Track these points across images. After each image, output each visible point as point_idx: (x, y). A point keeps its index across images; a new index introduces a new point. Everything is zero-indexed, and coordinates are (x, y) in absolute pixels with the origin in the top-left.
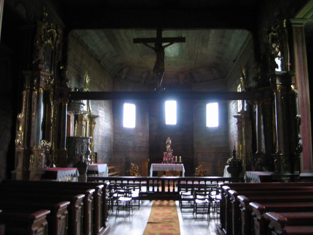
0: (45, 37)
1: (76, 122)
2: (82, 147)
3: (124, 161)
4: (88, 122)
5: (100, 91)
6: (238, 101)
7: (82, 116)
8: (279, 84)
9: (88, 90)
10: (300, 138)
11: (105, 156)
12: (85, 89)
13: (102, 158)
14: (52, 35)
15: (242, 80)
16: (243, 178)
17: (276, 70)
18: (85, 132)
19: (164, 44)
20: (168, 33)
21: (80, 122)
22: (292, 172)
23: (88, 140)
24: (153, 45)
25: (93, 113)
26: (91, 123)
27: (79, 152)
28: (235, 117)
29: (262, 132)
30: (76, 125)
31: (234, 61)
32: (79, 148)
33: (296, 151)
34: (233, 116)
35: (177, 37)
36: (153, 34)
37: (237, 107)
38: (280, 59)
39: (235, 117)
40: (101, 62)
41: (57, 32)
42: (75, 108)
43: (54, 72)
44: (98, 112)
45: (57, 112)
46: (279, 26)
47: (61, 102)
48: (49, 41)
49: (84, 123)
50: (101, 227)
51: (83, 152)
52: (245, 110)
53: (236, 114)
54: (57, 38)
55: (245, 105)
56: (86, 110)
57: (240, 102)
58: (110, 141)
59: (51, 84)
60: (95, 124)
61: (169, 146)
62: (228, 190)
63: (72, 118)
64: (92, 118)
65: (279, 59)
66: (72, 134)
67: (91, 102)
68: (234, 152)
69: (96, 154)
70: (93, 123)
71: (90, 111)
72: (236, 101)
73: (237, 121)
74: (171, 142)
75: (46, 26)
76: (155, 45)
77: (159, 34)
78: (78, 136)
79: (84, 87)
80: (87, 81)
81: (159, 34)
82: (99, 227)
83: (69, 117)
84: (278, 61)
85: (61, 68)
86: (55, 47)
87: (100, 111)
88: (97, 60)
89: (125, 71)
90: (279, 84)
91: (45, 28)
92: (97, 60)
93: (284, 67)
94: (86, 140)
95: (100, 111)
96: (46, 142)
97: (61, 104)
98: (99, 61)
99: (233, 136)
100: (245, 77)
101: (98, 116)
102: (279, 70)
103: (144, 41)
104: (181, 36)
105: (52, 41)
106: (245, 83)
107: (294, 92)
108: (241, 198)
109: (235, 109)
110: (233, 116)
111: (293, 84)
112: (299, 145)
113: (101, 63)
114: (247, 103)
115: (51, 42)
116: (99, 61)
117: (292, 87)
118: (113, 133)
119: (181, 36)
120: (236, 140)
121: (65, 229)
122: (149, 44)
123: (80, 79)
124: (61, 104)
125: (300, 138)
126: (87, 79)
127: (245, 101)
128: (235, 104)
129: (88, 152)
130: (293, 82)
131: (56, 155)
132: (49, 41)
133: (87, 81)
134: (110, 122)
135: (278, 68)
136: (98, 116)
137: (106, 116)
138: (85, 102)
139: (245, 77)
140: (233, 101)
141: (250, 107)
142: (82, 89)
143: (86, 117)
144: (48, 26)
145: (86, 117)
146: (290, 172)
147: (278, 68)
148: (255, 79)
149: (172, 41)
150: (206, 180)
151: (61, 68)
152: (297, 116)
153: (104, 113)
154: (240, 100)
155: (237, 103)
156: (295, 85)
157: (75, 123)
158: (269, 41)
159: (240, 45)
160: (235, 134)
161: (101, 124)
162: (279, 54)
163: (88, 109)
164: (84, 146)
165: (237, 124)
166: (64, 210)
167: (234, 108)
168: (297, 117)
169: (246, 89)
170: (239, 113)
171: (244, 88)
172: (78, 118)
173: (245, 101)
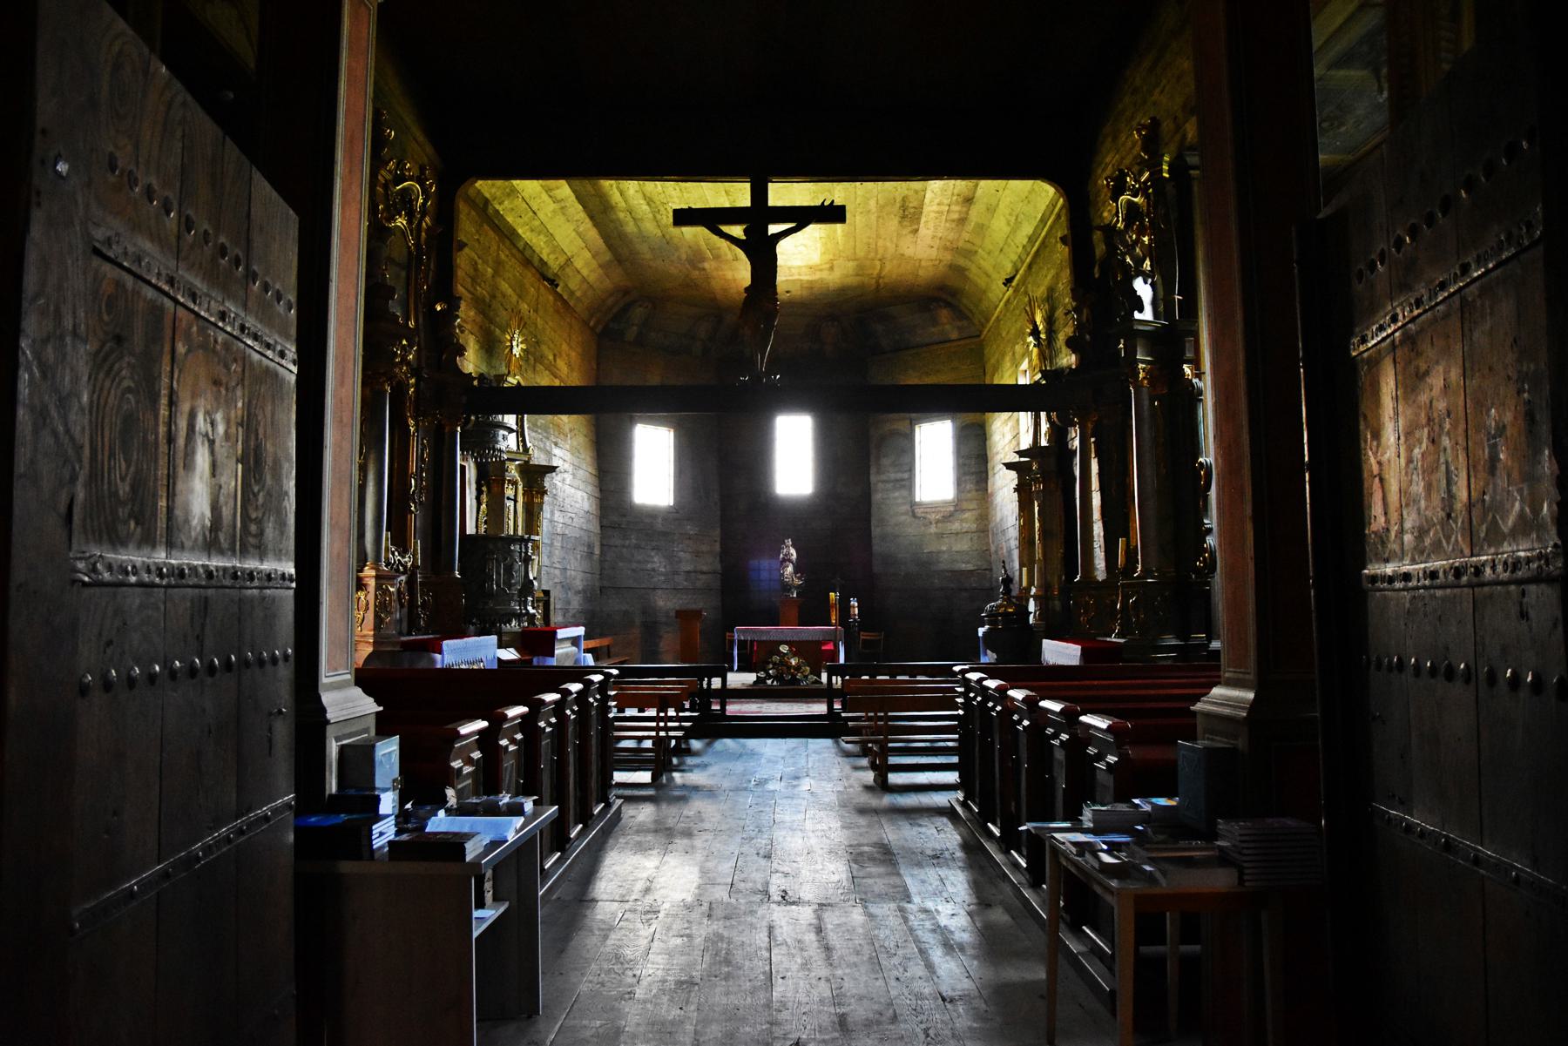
0: (387, 208)
1: (484, 489)
2: (509, 570)
3: (638, 621)
4: (520, 488)
5: (557, 383)
6: (1022, 414)
7: (501, 467)
8: (1143, 362)
9: (519, 383)
10: (1209, 531)
11: (576, 603)
12: (510, 379)
13: (565, 611)
14: (411, 201)
15: (1035, 346)
16: (1027, 608)
17: (1137, 315)
18: (514, 521)
19: (774, 229)
20: (782, 194)
21: (495, 489)
22: (1183, 634)
23: (527, 548)
24: (737, 231)
25: (538, 458)
26: (531, 491)
27: (498, 585)
28: (1009, 466)
29: (1096, 515)
30: (484, 498)
31: (1008, 282)
32: (498, 574)
33: (1197, 571)
34: (1004, 464)
35: (818, 203)
36: (738, 194)
37: (1016, 436)
38: (1150, 281)
39: (1009, 466)
40: (557, 286)
41: (425, 191)
42: (481, 441)
43: (416, 322)
44: (549, 454)
45: (428, 455)
46: (1147, 174)
47: (439, 422)
48: (401, 222)
49: (509, 492)
50: (598, 803)
51: (510, 586)
52: (1044, 443)
53: (1016, 459)
54: (424, 213)
55: (1044, 426)
56: (515, 449)
57: (1025, 418)
58: (591, 553)
59: (409, 362)
60: (543, 492)
61: (790, 569)
62: (980, 680)
63: (471, 474)
64: (535, 477)
65: (1146, 282)
66: (470, 529)
67: (528, 421)
68: (1008, 581)
69: (547, 593)
70: (537, 492)
71: (526, 450)
72: (1016, 413)
73: (1016, 482)
74: (795, 554)
75: (390, 171)
76: (745, 231)
77: (759, 194)
78: (491, 532)
79: (504, 370)
80: (517, 351)
81: (759, 194)
82: (571, 824)
83: (463, 468)
84: (1143, 289)
85: (439, 308)
86: (417, 238)
87: (556, 451)
88: (545, 278)
89: (638, 313)
90: (1143, 362)
91: (389, 177)
92: (545, 278)
93: (1161, 308)
94: (521, 548)
95: (556, 451)
96: (396, 553)
97: (440, 427)
98: (553, 283)
99: (1004, 532)
100: (1043, 336)
101: (553, 469)
102: (1147, 314)
103: (712, 218)
104: (833, 201)
105: (410, 222)
106: (1042, 356)
107: (1192, 385)
108: (1018, 694)
109: (1011, 441)
110: (1004, 464)
111: (1187, 362)
112: (1205, 550)
113: (559, 289)
114: (1049, 418)
115: (405, 222)
116: (553, 283)
117: (1187, 369)
118: (599, 528)
119: (833, 201)
120: (1014, 543)
121: (517, 782)
122: (725, 229)
123: (491, 346)
124: (440, 427)
125: (1209, 531)
126: (515, 343)
127: (1043, 415)
128: (1010, 424)
129: (527, 585)
130: (1189, 355)
131: (428, 596)
132: (401, 222)
133: (514, 351)
134: (590, 488)
135: (1141, 310)
136: (553, 469)
137: (577, 467)
138: (510, 420)
139: (1043, 336)
140: (1005, 415)
141: (1058, 434)
142: (501, 378)
143: (513, 472)
144: (396, 170)
145: (513, 472)
146: (1178, 638)
147: (1141, 310)
148: (1072, 344)
149: (801, 217)
150: (913, 671)
151: (439, 308)
152: (1200, 459)
153: (568, 456)
154: (1027, 411)
155: (1018, 420)
156: (1196, 363)
157: (479, 492)
158: (1118, 221)
159: (1027, 229)
160: (1009, 525)
161: (560, 494)
162: (1147, 265)
163: (521, 444)
164: (516, 567)
165: (1015, 490)
166: (514, 729)
167: (1009, 437)
168: (1201, 463)
169: (1045, 374)
170: (1021, 453)
171: (1041, 371)
172: (491, 478)
173: (1043, 415)
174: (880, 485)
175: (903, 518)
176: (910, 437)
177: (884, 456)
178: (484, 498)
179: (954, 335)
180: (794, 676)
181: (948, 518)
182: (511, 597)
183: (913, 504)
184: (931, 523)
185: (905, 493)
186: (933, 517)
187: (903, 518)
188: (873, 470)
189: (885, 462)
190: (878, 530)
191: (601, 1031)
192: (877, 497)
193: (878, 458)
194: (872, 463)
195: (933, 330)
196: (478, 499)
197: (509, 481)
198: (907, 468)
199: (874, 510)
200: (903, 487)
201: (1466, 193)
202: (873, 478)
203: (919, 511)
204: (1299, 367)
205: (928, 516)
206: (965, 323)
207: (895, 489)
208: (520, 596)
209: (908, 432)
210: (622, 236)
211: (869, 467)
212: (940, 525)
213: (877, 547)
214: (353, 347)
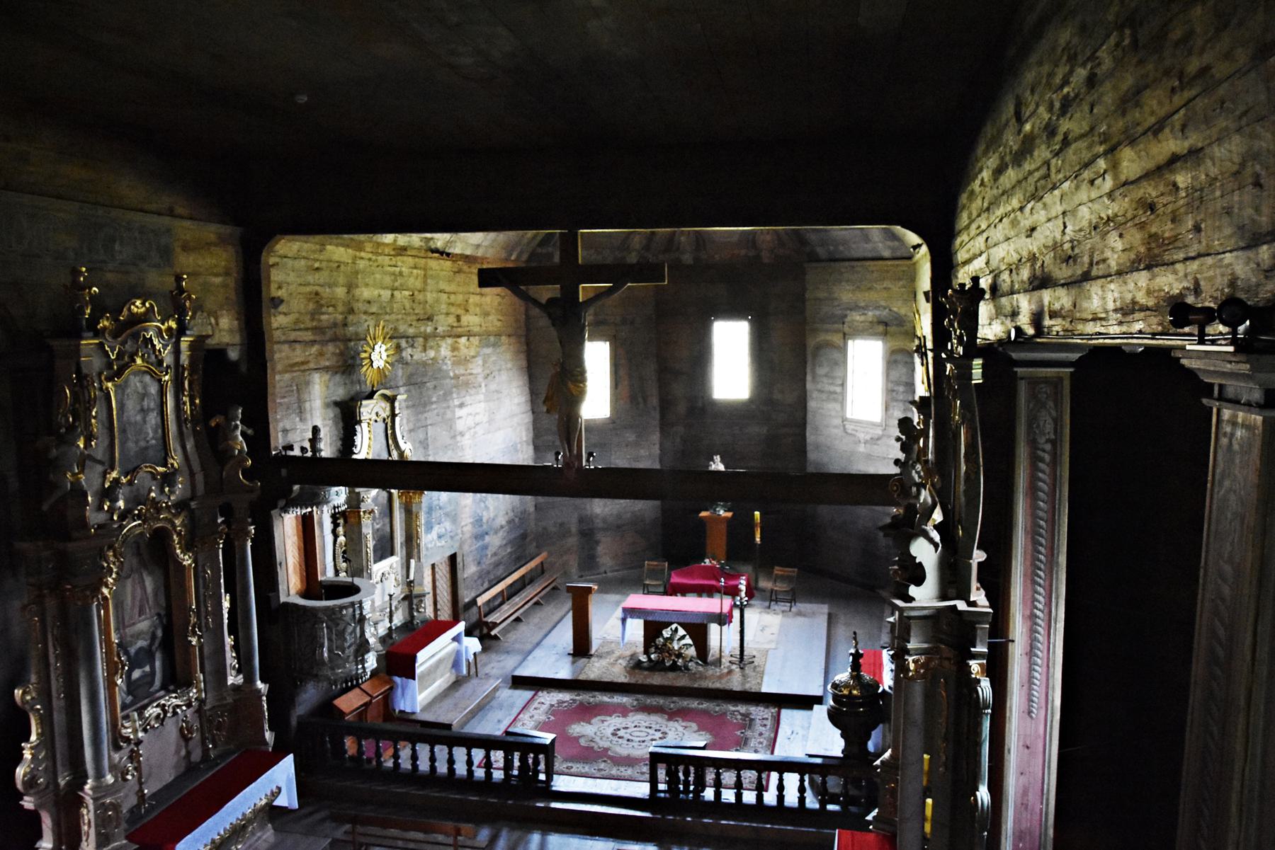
3: (574, 529)
30: (341, 530)
174: (815, 394)
175: (836, 431)
176: (843, 350)
177: (819, 366)
178: (341, 530)
179: (887, 254)
180: (675, 662)
181: (875, 440)
182: (347, 660)
183: (844, 420)
184: (860, 441)
185: (837, 406)
186: (861, 436)
187: (836, 431)
188: (809, 378)
189: (821, 371)
190: (813, 437)
191: (855, 324)
192: (812, 405)
193: (814, 365)
194: (808, 370)
195: (866, 246)
196: (334, 532)
197: (364, 512)
198: (840, 383)
199: (809, 416)
200: (835, 400)
201: (670, 815)
202: (809, 386)
203: (849, 427)
204: (675, 815)
205: (858, 434)
206: (896, 243)
207: (828, 400)
208: (356, 657)
209: (842, 345)
210: (532, 368)
211: (805, 374)
212: (868, 445)
213: (812, 456)
214: (389, 845)
